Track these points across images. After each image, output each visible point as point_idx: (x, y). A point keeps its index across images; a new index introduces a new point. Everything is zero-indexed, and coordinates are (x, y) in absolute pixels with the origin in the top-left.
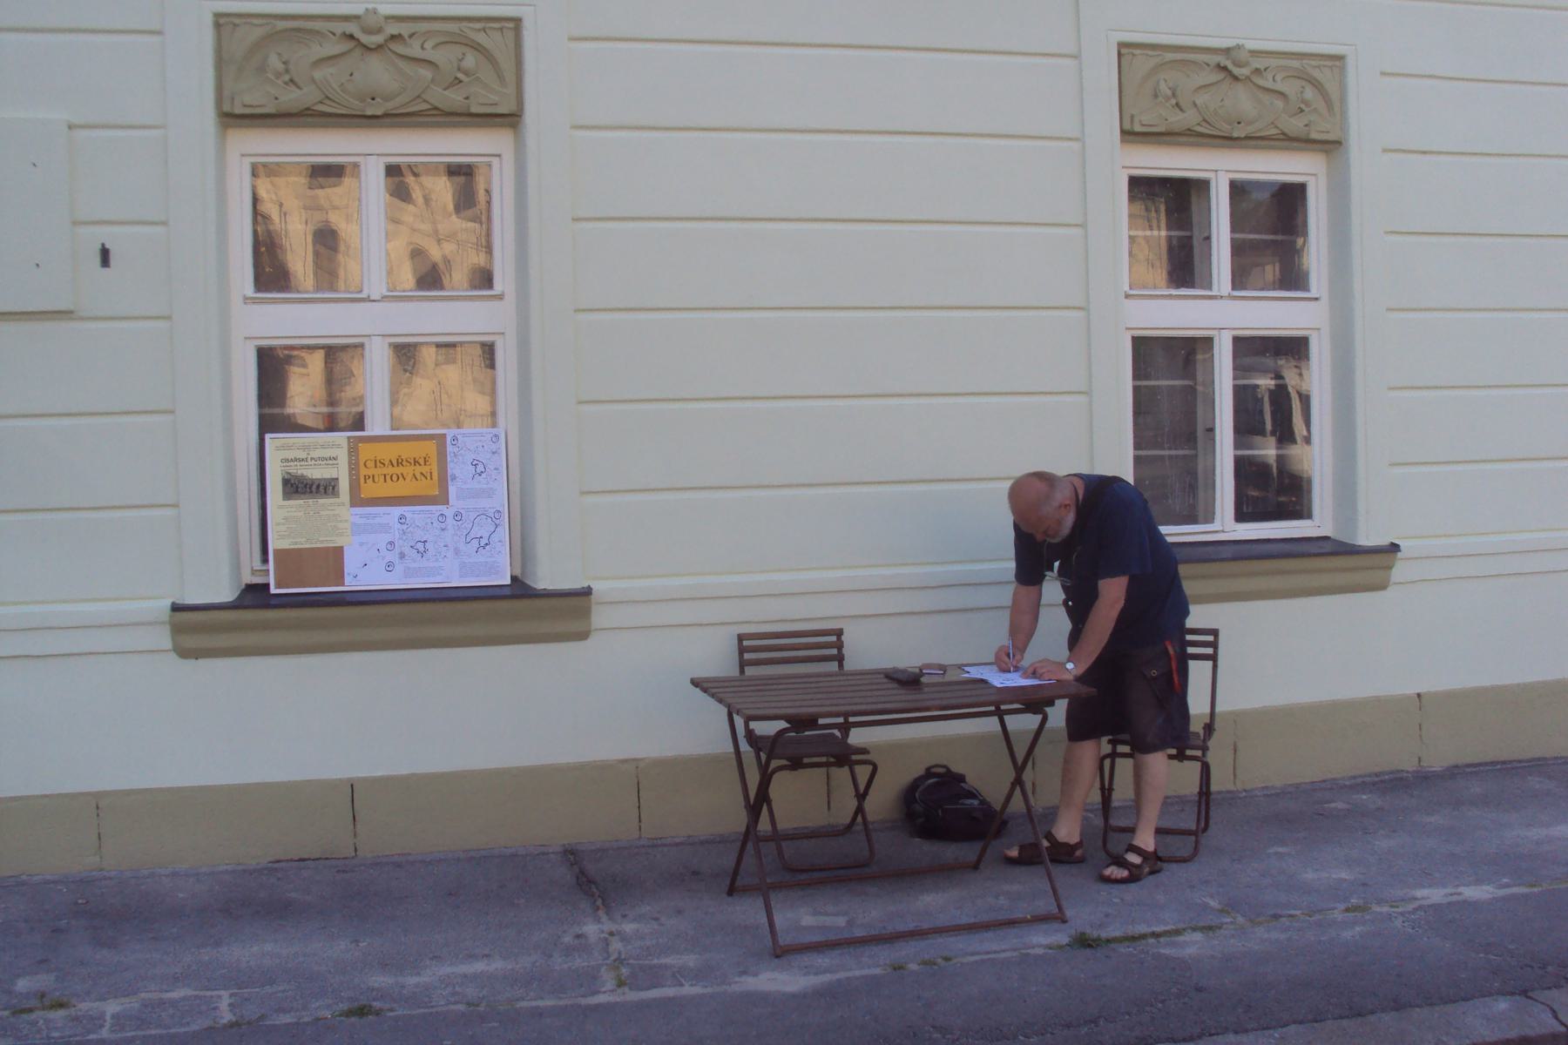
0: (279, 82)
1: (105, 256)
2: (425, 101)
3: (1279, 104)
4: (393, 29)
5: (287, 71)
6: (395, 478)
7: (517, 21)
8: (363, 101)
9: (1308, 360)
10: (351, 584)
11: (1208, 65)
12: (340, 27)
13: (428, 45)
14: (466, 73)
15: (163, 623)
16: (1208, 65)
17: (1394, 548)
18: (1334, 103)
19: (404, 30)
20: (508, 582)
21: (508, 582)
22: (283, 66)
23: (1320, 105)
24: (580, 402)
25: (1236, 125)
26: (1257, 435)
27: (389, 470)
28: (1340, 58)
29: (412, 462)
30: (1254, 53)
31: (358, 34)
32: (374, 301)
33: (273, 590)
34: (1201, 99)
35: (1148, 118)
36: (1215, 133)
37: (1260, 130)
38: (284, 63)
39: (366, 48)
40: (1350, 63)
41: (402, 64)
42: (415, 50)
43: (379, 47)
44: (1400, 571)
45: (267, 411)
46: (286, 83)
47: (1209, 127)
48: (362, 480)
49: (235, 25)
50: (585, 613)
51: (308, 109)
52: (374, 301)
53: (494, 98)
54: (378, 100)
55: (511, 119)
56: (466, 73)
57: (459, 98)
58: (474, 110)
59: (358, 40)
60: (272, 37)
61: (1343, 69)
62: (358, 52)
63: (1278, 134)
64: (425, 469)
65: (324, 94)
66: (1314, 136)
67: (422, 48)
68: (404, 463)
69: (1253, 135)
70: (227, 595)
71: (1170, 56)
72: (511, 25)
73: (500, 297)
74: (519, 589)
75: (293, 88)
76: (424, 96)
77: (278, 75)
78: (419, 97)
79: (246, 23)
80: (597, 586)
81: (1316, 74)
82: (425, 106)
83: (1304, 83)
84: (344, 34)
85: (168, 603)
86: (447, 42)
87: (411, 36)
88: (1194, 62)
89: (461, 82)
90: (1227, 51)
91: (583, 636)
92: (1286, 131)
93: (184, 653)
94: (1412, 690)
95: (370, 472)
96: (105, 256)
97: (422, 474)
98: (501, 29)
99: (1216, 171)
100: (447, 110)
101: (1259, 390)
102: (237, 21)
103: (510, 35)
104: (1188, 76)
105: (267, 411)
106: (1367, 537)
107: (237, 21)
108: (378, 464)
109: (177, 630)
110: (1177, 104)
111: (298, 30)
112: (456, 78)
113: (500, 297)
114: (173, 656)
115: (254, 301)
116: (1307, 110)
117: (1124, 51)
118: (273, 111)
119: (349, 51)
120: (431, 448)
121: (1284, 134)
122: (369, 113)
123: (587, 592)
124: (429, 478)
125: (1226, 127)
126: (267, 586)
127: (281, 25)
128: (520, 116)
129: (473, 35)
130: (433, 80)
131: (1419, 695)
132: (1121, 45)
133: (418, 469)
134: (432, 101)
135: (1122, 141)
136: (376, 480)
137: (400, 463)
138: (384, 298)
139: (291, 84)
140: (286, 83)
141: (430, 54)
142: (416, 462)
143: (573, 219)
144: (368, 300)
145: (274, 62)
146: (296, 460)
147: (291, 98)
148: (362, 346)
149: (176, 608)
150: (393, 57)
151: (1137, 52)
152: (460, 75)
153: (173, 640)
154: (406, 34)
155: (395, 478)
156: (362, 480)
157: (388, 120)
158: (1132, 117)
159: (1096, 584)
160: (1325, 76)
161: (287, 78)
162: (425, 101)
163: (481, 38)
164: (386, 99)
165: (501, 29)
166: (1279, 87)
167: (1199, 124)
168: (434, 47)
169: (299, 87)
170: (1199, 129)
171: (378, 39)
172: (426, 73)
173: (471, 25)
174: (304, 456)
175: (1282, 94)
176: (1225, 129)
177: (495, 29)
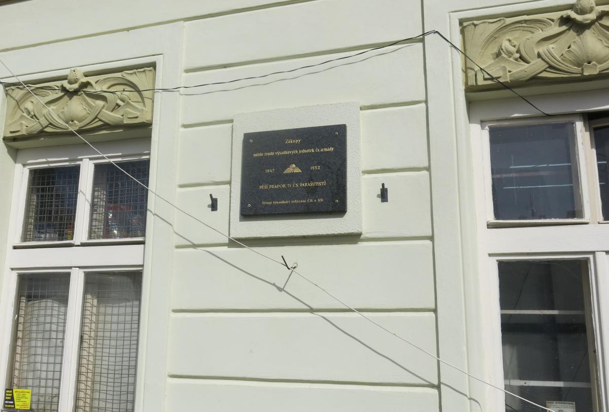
0: (511, 59)
1: (384, 195)
8: (67, 123)
9: (501, 314)
11: (553, 20)
16: (553, 20)
31: (573, 14)
34: (542, 49)
41: (89, 100)
42: (97, 88)
46: (516, 60)
49: (475, 25)
53: (138, 114)
57: (119, 116)
65: (547, 63)
72: (151, 68)
75: (523, 63)
78: (96, 117)
79: (483, 23)
82: (100, 123)
96: (384, 195)
102: (475, 22)
104: (533, 33)
107: (475, 22)
127: (509, 21)
139: (519, 60)
140: (516, 60)
162: (100, 120)
164: (600, 62)
167: (545, 70)
169: (527, 62)
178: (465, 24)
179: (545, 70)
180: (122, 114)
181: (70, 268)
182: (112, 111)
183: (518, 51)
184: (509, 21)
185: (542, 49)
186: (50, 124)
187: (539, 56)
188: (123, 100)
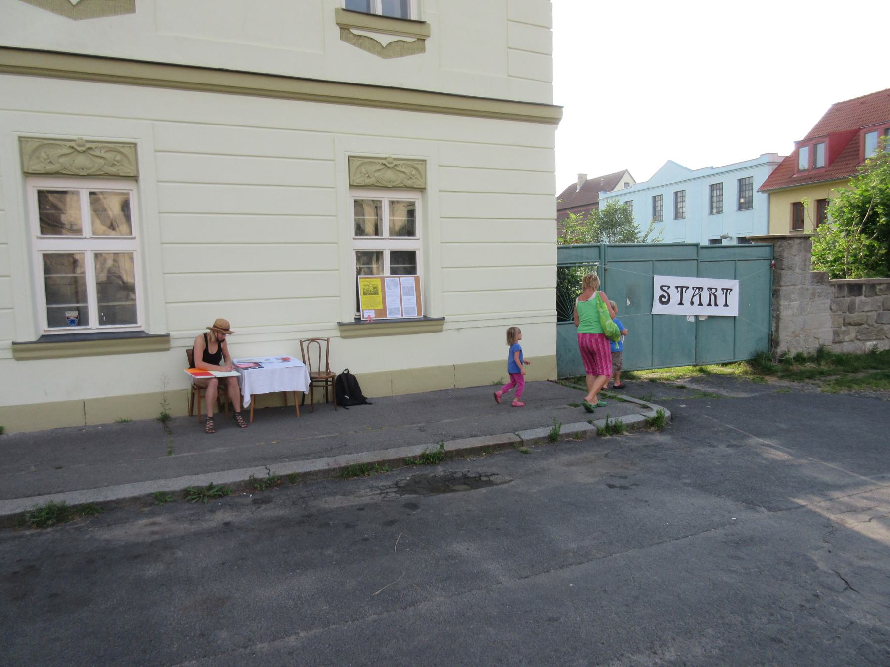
3: (404, 176)
4: (89, 145)
5: (367, 173)
7: (136, 144)
8: (387, 182)
10: (389, 317)
11: (66, 146)
12: (381, 161)
13: (403, 167)
14: (413, 176)
15: (8, 349)
17: (443, 319)
18: (423, 175)
19: (93, 145)
22: (47, 157)
23: (418, 176)
24: (442, 268)
25: (81, 170)
28: (425, 161)
30: (87, 141)
31: (75, 147)
33: (362, 319)
35: (359, 180)
36: (379, 185)
37: (93, 172)
38: (48, 155)
39: (79, 152)
40: (428, 162)
41: (93, 158)
42: (97, 153)
43: (84, 152)
44: (445, 326)
45: (47, 276)
49: (27, 141)
50: (168, 342)
54: (84, 170)
55: (422, 190)
56: (118, 162)
58: (121, 174)
60: (42, 146)
61: (425, 164)
62: (76, 153)
66: (415, 186)
67: (100, 152)
69: (397, 186)
70: (33, 338)
71: (366, 160)
72: (133, 145)
73: (134, 238)
74: (426, 319)
75: (52, 165)
76: (102, 169)
77: (45, 160)
80: (172, 333)
81: (417, 166)
83: (412, 169)
84: (70, 146)
85: (11, 342)
87: (96, 148)
88: (375, 162)
89: (115, 165)
90: (385, 158)
91: (168, 349)
93: (18, 359)
94: (452, 364)
98: (130, 147)
100: (111, 174)
103: (134, 149)
105: (47, 276)
106: (434, 314)
109: (15, 351)
110: (369, 176)
111: (52, 144)
112: (114, 163)
113: (134, 238)
114: (14, 361)
115: (41, 238)
116: (413, 178)
117: (350, 158)
118: (44, 172)
119: (73, 152)
122: (81, 174)
123: (167, 336)
125: (385, 183)
126: (360, 318)
127: (46, 142)
128: (138, 177)
129: (415, 165)
130: (105, 164)
131: (454, 365)
132: (349, 157)
134: (105, 171)
135: (350, 188)
138: (92, 238)
141: (103, 154)
143: (159, 213)
144: (85, 238)
145: (43, 155)
147: (51, 168)
148: (84, 254)
149: (14, 344)
150: (91, 156)
151: (355, 159)
152: (115, 163)
153: (13, 354)
154: (94, 147)
157: (392, 189)
158: (353, 181)
160: (420, 167)
163: (122, 150)
165: (130, 147)
166: (402, 170)
170: (377, 185)
171: (83, 149)
172: (102, 161)
173: (118, 145)
175: (404, 173)
176: (385, 184)
177: (127, 147)
178: (22, 139)
181: (86, 251)
183: (49, 158)
184: (46, 142)
185: (376, 175)
186: (65, 168)
187: (59, 162)
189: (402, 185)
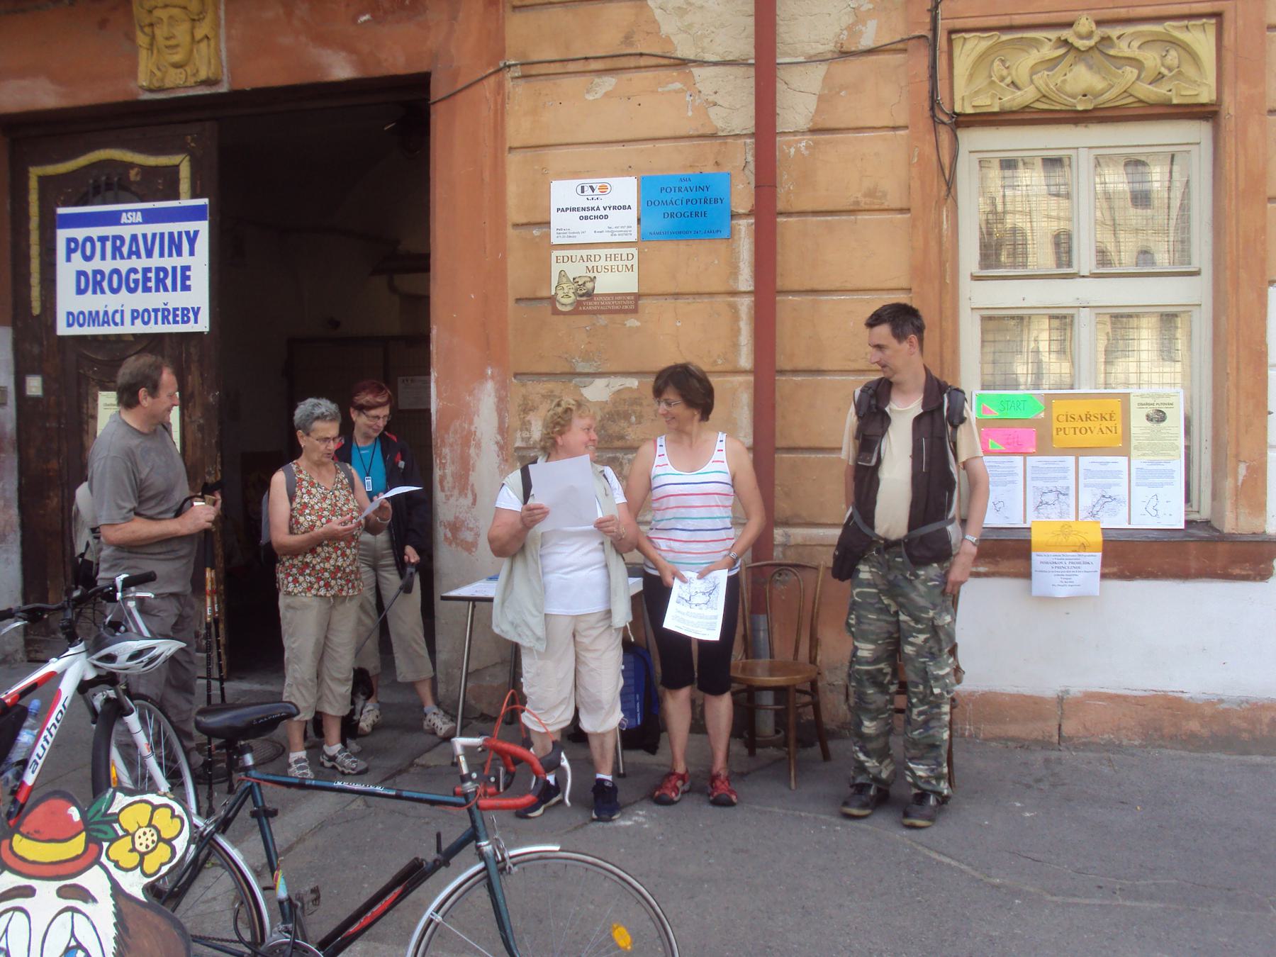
2: (1131, 95)
6: (1083, 431)
20: (1182, 526)
21: (1182, 526)
26: (1266, 442)
27: (1079, 424)
29: (1099, 417)
32: (1083, 277)
46: (1008, 86)
47: (1047, 101)
48: (1055, 432)
49: (965, 39)
51: (1027, 106)
52: (1083, 277)
59: (1072, 44)
63: (1135, 102)
64: (1109, 424)
65: (1041, 92)
68: (1092, 418)
78: (1125, 91)
86: (1148, 42)
87: (1119, 38)
89: (1163, 76)
92: (1142, 97)
95: (1062, 425)
97: (1108, 428)
99: (1078, 148)
101: (697, 417)
108: (1069, 419)
120: (1116, 405)
121: (1141, 101)
124: (1114, 431)
129: (1177, 34)
133: (1105, 423)
136: (1067, 432)
137: (1088, 418)
139: (1011, 86)
142: (1103, 418)
146: (1147, 404)
155: (1083, 431)
156: (1055, 432)
159: (666, 630)
161: (1008, 80)
167: (1038, 100)
168: (1139, 47)
174: (1153, 402)
179: (1038, 100)
180: (1168, 89)
182: (1150, 84)
186: (1044, 96)
188: (1170, 70)
189: (1130, 100)
